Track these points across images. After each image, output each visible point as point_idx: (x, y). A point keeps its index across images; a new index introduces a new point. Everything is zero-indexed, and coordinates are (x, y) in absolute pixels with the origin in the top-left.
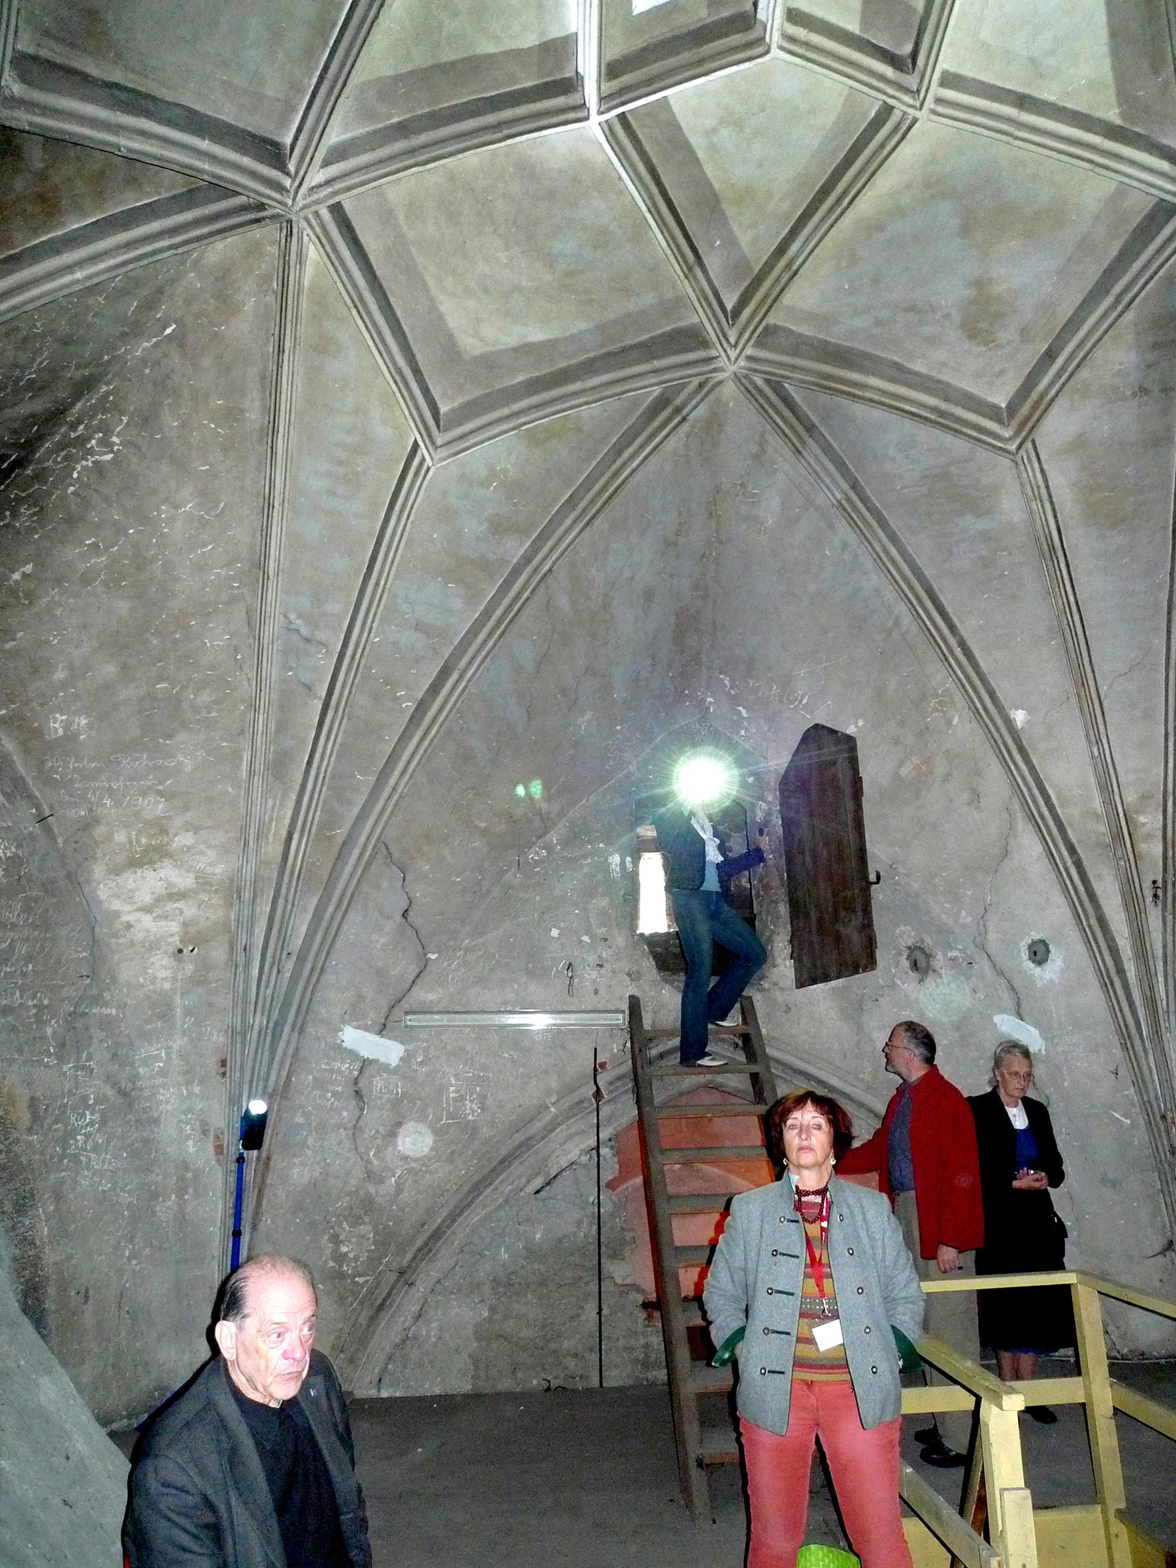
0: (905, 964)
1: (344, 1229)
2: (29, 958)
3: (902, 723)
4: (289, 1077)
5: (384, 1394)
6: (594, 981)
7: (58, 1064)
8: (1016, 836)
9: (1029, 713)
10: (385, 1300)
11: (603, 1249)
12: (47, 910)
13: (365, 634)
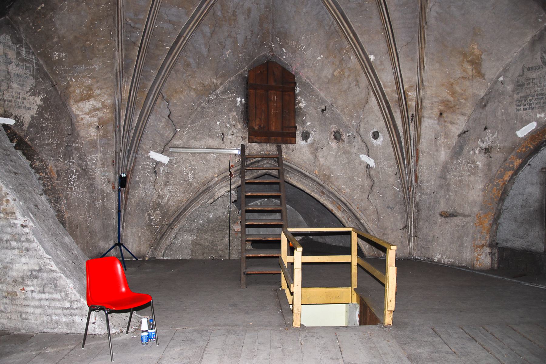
0: (333, 137)
1: (152, 212)
2: (53, 129)
3: (335, 57)
4: (133, 167)
5: (165, 258)
6: (230, 139)
7: (64, 161)
8: (370, 97)
9: (375, 56)
10: (165, 233)
11: (231, 221)
12: (57, 114)
13: (152, 26)
